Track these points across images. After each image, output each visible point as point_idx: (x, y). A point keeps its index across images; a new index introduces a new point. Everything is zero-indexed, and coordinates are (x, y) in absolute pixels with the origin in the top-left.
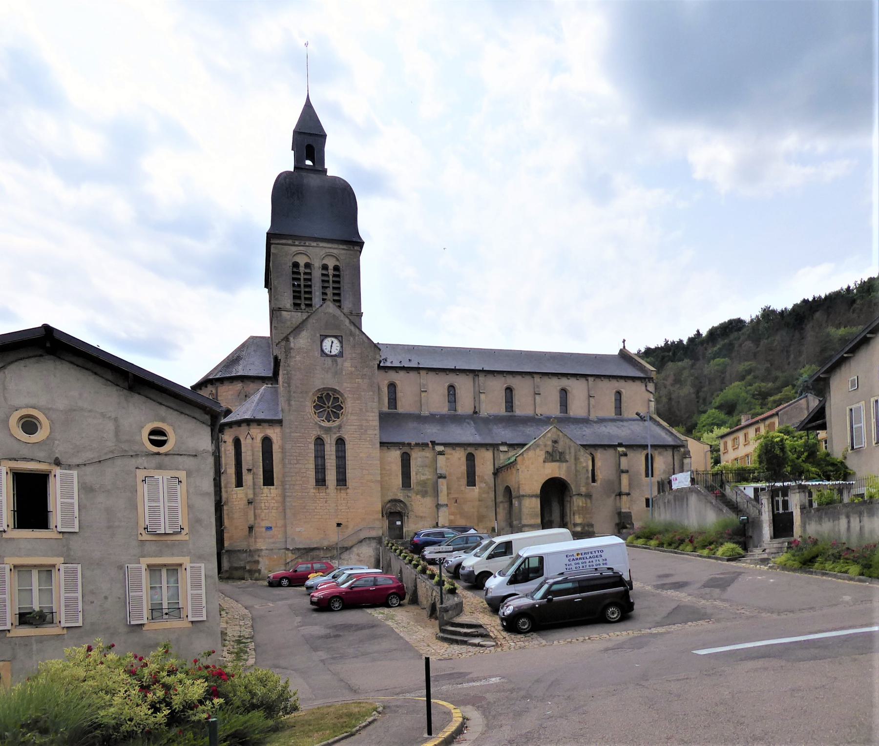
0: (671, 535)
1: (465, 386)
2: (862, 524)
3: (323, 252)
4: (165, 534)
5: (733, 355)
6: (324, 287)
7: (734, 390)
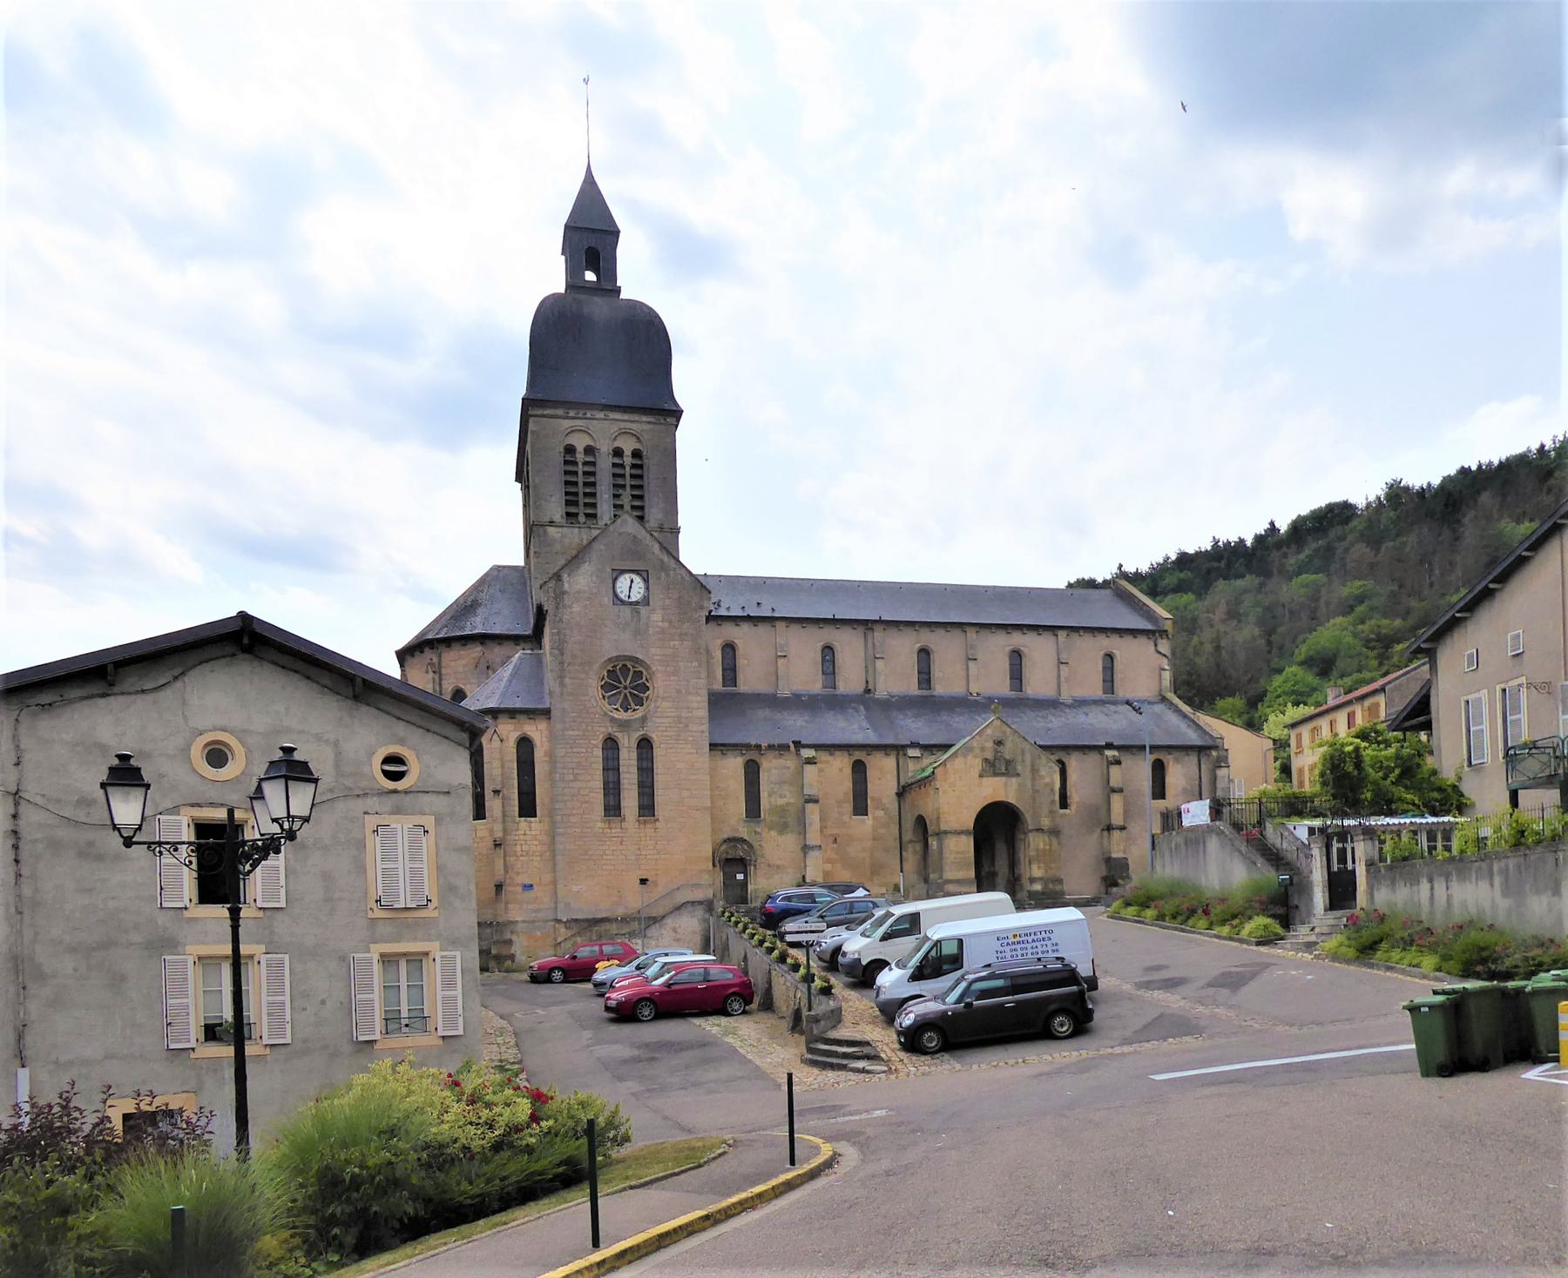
0: (1177, 901)
1: (850, 647)
2: (1449, 892)
3: (614, 428)
4: (406, 908)
5: (1334, 567)
6: (616, 496)
7: (1332, 632)
